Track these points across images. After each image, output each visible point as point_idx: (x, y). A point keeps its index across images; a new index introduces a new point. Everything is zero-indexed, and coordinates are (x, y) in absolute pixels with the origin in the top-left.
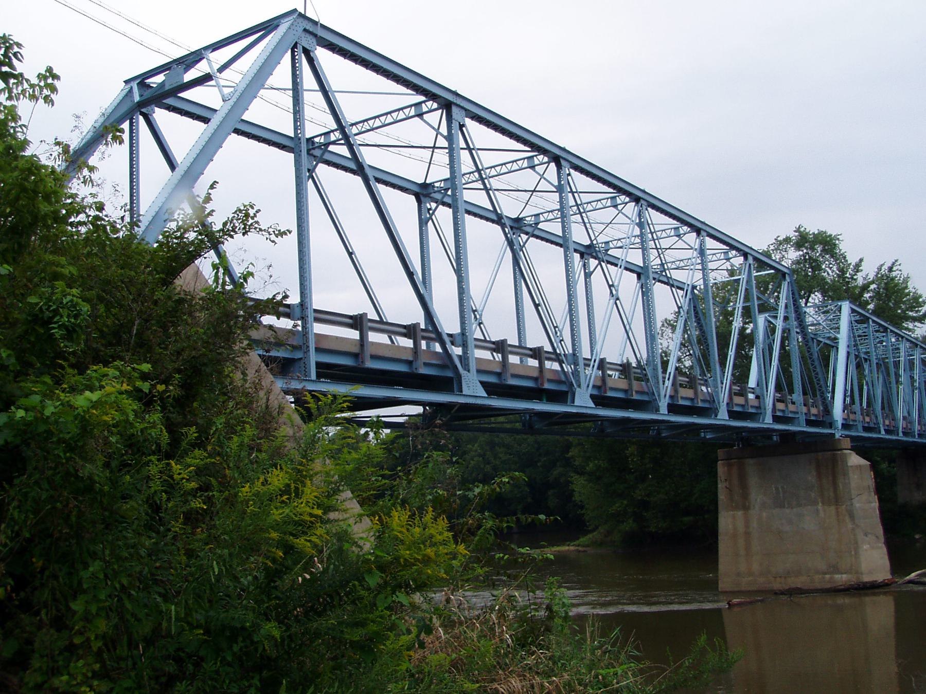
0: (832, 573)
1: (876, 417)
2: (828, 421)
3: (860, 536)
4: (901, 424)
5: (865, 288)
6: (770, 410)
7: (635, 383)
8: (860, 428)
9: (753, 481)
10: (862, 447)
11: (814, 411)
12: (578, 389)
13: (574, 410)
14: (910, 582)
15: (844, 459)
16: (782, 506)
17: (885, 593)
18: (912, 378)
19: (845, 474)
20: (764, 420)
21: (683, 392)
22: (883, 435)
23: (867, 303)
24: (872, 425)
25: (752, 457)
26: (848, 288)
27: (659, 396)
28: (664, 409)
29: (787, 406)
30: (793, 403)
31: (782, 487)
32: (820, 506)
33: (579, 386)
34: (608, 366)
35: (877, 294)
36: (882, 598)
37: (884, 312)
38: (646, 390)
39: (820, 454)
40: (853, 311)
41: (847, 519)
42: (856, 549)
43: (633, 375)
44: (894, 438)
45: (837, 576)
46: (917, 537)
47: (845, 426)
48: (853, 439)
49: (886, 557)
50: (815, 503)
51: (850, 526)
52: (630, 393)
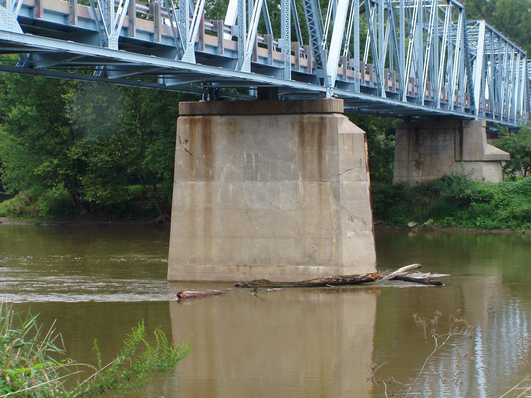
2: (472, 109)
3: (345, 220)
4: (407, 87)
8: (357, 88)
9: (220, 143)
10: (357, 112)
11: (303, 62)
14: (396, 278)
15: (334, 128)
16: (253, 178)
17: (367, 290)
18: (425, 31)
19: (334, 143)
20: (240, 68)
22: (384, 99)
24: (372, 85)
25: (222, 115)
27: (109, 26)
28: (114, 44)
29: (270, 53)
30: (279, 50)
31: (256, 155)
32: (300, 182)
39: (307, 116)
41: (331, 199)
46: (411, 224)
47: (340, 84)
48: (347, 101)
49: (373, 247)
51: (334, 207)
52: (70, 18)
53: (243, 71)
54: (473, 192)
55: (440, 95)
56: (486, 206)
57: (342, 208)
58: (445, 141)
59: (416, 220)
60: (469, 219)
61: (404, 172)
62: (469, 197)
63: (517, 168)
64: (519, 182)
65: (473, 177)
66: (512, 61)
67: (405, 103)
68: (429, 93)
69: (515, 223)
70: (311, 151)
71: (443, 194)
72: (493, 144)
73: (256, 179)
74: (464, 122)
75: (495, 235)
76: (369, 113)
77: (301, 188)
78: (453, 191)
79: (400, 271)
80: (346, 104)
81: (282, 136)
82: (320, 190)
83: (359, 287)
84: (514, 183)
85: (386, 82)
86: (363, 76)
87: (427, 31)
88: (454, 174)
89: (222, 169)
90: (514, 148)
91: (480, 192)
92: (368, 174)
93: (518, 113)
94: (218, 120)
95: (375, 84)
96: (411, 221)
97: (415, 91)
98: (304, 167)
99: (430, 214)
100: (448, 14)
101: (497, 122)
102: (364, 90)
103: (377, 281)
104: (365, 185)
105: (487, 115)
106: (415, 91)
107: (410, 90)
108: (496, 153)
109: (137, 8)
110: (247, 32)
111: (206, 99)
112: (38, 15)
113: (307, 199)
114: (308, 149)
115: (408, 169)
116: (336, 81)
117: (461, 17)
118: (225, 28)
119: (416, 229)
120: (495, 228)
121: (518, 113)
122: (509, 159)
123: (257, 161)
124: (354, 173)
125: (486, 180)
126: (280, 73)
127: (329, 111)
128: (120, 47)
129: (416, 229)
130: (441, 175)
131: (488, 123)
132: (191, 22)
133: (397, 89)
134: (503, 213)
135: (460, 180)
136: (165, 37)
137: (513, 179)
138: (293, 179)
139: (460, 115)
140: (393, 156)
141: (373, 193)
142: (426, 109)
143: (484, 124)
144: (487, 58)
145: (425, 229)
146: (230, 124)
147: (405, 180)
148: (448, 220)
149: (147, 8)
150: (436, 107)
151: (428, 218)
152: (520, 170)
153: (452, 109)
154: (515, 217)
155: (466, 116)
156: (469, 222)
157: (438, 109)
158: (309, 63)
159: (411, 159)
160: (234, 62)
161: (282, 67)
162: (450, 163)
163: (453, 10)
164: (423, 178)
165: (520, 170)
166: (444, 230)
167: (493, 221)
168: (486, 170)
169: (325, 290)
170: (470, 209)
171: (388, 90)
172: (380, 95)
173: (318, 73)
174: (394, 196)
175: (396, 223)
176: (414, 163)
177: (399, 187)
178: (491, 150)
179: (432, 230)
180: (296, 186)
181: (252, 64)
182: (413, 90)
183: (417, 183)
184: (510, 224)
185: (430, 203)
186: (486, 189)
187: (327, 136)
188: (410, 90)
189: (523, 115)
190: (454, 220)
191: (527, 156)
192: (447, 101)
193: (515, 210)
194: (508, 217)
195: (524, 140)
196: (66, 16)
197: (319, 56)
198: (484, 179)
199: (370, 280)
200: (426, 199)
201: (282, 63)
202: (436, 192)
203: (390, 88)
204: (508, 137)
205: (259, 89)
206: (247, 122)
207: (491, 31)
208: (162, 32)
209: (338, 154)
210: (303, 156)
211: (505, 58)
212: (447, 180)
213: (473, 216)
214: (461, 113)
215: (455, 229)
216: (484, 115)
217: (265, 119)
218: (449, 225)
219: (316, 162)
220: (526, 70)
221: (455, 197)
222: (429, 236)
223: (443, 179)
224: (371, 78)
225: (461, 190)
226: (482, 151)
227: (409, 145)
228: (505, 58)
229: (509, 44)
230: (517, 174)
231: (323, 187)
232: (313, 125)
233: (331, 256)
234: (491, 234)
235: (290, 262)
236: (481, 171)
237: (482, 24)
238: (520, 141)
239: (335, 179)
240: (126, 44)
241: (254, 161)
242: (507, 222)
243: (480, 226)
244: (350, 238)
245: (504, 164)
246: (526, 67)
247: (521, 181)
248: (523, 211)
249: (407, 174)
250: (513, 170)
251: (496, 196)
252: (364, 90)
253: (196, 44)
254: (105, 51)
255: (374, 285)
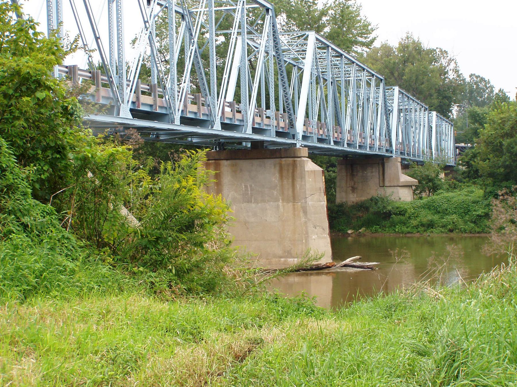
0: (287, 257)
1: (328, 130)
2: (292, 133)
3: (311, 228)
4: (347, 137)
5: (323, 13)
6: (251, 123)
7: (158, 99)
8: (315, 140)
9: (227, 179)
10: (315, 155)
11: (282, 124)
12: (122, 105)
13: (120, 121)
14: (345, 266)
15: (302, 167)
16: (249, 201)
17: (327, 274)
18: (358, 96)
19: (302, 177)
20: (245, 131)
21: (145, 99)
22: (332, 146)
23: (324, 26)
24: (324, 137)
25: (227, 160)
26: (309, 11)
27: (175, 110)
28: (177, 121)
29: (262, 120)
30: (268, 117)
31: (251, 186)
32: (280, 203)
33: (123, 102)
34: (79, 72)
35: (334, 18)
36: (324, 277)
37: (338, 36)
38: (165, 106)
39: (284, 159)
40: (317, 39)
41: (302, 214)
42: (307, 238)
43: (100, 81)
44: (340, 148)
45: (290, 260)
46: (350, 232)
47: (305, 138)
48: (310, 148)
49: (329, 245)
50: (277, 200)
51: (303, 220)
52: (154, 107)
53: (248, 133)
54: (393, 208)
55: (369, 141)
56: (402, 218)
57: (309, 220)
58: (372, 172)
59: (353, 228)
60: (390, 227)
61: (344, 194)
62: (390, 211)
63: (423, 190)
64: (425, 201)
65: (392, 198)
66: (417, 113)
67: (346, 148)
68: (362, 140)
69: (423, 229)
70: (287, 183)
71: (371, 210)
72: (406, 174)
73: (251, 202)
74: (385, 159)
75: (409, 237)
76: (319, 154)
77: (281, 207)
78: (379, 208)
79: (348, 261)
80: (138, 130)
81: (268, 173)
82: (294, 208)
83: (322, 271)
84: (422, 201)
85: (333, 134)
86: (318, 131)
87: (359, 96)
88: (379, 196)
89: (228, 195)
90: (421, 176)
91: (397, 208)
92: (325, 197)
93: (423, 151)
94: (225, 163)
95: (326, 136)
96: (350, 229)
97: (352, 139)
98: (283, 193)
99: (363, 224)
100: (373, 83)
101: (408, 158)
102: (320, 140)
103: (333, 268)
104: (323, 204)
105: (401, 153)
106: (352, 139)
107: (349, 139)
108: (408, 180)
109: (142, 88)
110: (218, 100)
111: (216, 149)
112: (139, 107)
113: (285, 214)
114: (285, 182)
115: (346, 192)
116: (303, 136)
117: (382, 85)
118: (79, 72)
119: (353, 235)
120: (409, 233)
121: (423, 151)
122: (417, 184)
123: (251, 190)
124: (316, 197)
125: (402, 199)
126: (268, 132)
127: (299, 156)
128: (223, 128)
129: (353, 235)
130: (370, 197)
131: (402, 159)
132: (178, 96)
133: (340, 139)
134: (414, 222)
135: (383, 199)
136: (161, 107)
137: (421, 198)
138: (276, 202)
139: (383, 154)
140: (335, 183)
141: (329, 209)
142: (359, 151)
143: (400, 160)
144: (400, 111)
145: (360, 235)
146: (233, 165)
147: (344, 200)
148: (376, 228)
149: (148, 87)
150: (366, 149)
151: (362, 227)
152: (425, 192)
153: (377, 151)
154: (423, 225)
155: (386, 155)
156: (390, 229)
157: (368, 151)
158: (285, 125)
159: (348, 186)
160: (241, 127)
161: (312, 135)
162: (376, 188)
163: (376, 80)
164: (357, 199)
165: (425, 192)
166: (374, 235)
167: (407, 228)
168: (401, 192)
169: (299, 275)
170: (391, 220)
171: (335, 140)
172: (330, 143)
173: (291, 132)
174: (337, 212)
175: (339, 231)
176: (351, 188)
177: (341, 205)
178: (405, 178)
179: (365, 235)
180: (278, 206)
181: (221, 123)
182: (351, 138)
183: (353, 202)
184: (419, 229)
185: (362, 216)
186: (402, 206)
187: (298, 172)
188: (349, 139)
189: (427, 152)
190: (380, 228)
191: (430, 182)
192: (374, 145)
193: (422, 220)
194: (418, 225)
195: (428, 170)
196: (151, 106)
197: (291, 120)
198: (400, 199)
199: (328, 267)
200: (360, 214)
201: (270, 125)
202: (367, 209)
203: (336, 138)
204: (416, 169)
205: (251, 142)
206: (244, 164)
207: (403, 94)
208: (202, 112)
209: (305, 185)
210: (282, 186)
211: (413, 111)
212: (374, 201)
213: (393, 225)
214: (383, 153)
215: (381, 234)
216: (399, 153)
217: (256, 162)
218: (376, 231)
219: (291, 190)
220: (428, 119)
221: (380, 211)
222: (363, 240)
223: (371, 200)
224: (324, 132)
225: (384, 206)
226: (398, 179)
227: (347, 176)
228: (413, 111)
229: (416, 102)
230: (424, 195)
231: (296, 206)
232: (288, 165)
233: (302, 252)
234: (406, 237)
235: (275, 256)
236: (398, 193)
237: (397, 89)
238: (425, 172)
239: (303, 201)
240: (185, 121)
241: (249, 190)
242: (417, 229)
243: (398, 232)
244: (314, 239)
245: (414, 188)
246: (428, 117)
247: (426, 200)
248: (428, 221)
249: (348, 197)
250: (421, 192)
251: (409, 211)
252: (320, 140)
253: (182, 111)
254: (118, 119)
255: (332, 270)
